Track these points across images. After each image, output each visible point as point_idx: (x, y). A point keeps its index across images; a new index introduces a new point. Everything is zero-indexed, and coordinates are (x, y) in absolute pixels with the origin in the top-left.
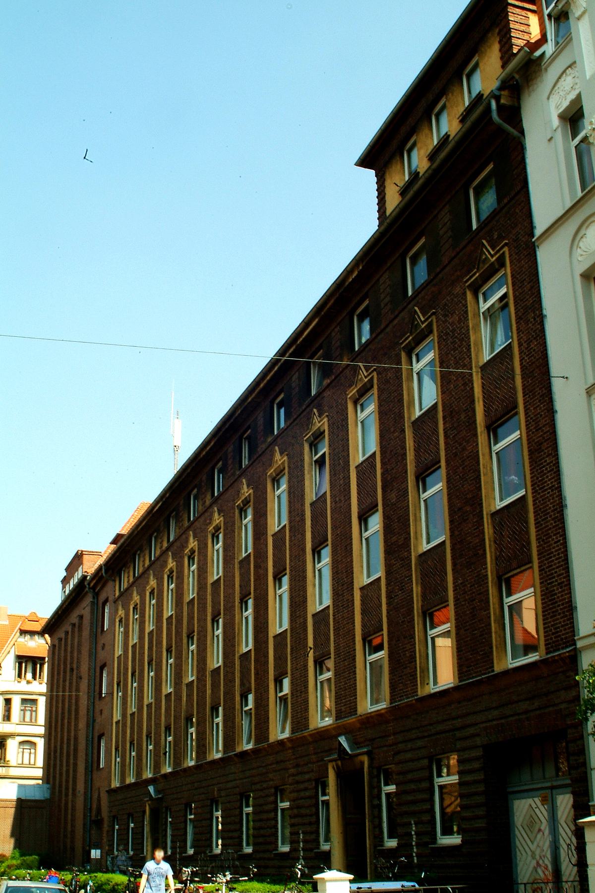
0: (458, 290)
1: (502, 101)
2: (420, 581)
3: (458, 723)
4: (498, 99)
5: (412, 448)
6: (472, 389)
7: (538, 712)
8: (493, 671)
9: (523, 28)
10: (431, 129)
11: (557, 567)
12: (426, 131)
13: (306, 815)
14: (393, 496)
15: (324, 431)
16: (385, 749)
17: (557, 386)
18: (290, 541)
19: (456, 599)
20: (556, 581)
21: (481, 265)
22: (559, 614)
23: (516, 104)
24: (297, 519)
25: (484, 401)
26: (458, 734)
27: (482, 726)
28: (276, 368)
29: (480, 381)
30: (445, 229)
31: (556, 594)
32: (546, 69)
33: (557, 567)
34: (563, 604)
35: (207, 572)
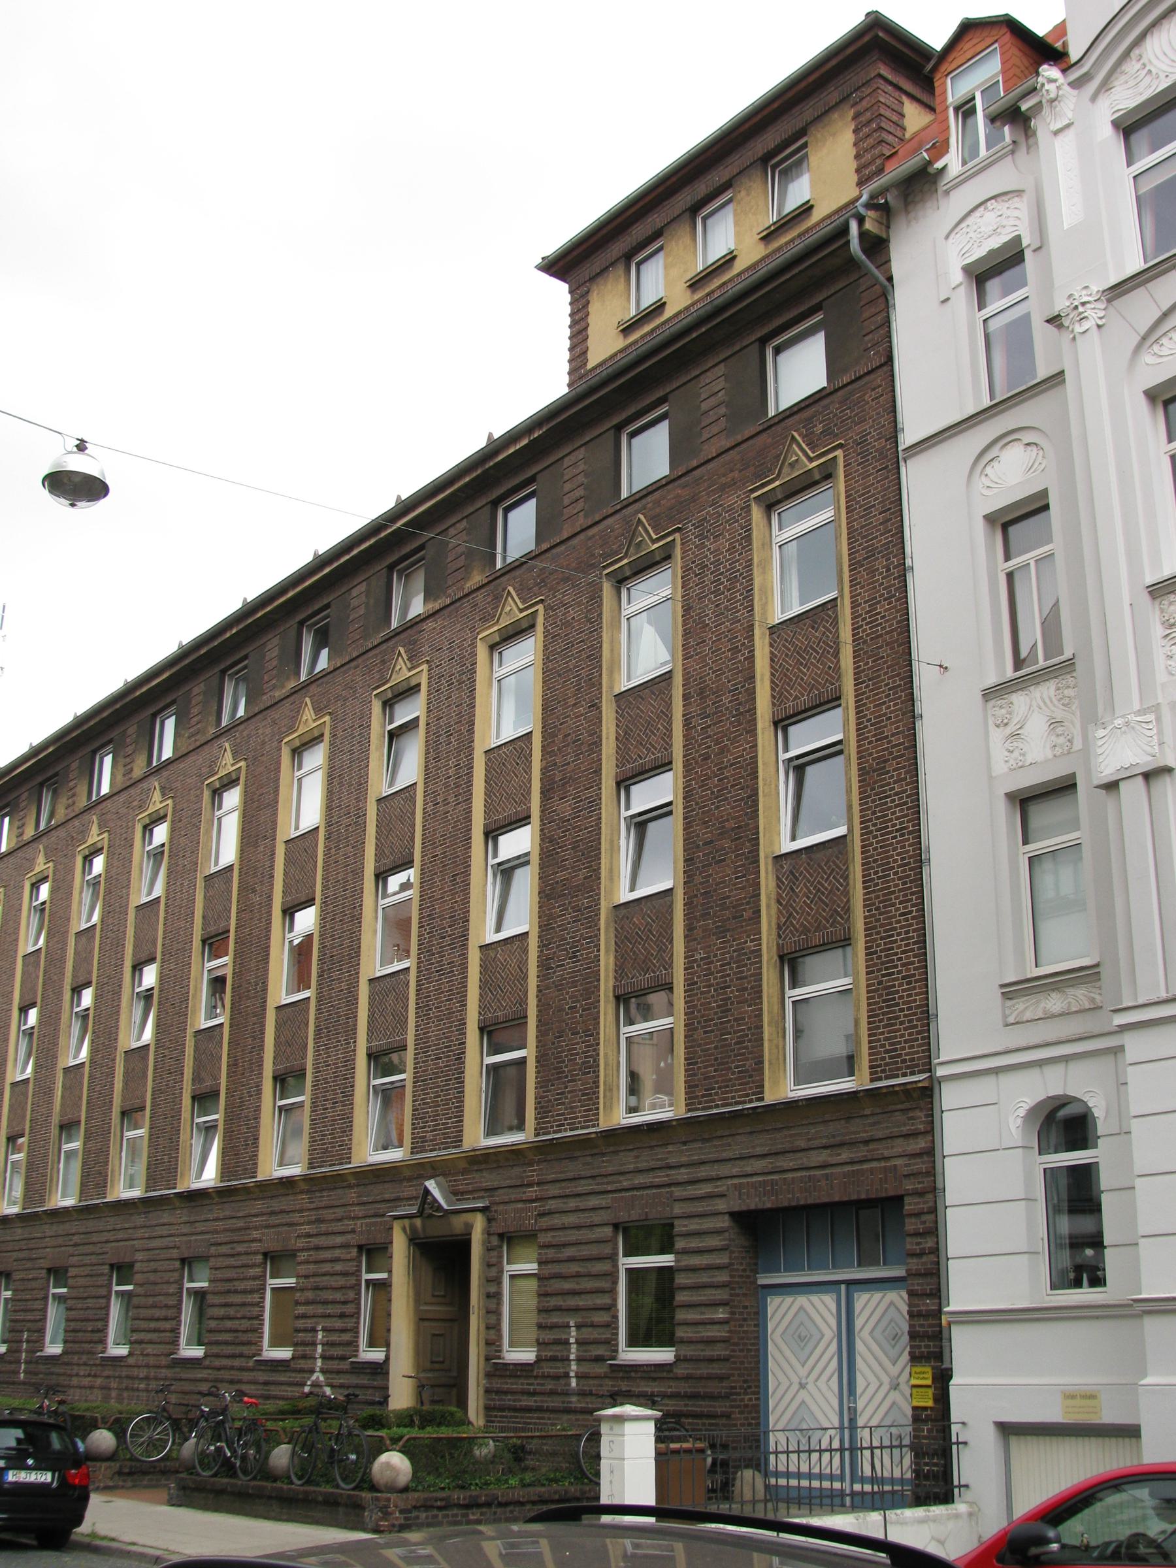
0: (733, 499)
1: (868, 225)
2: (613, 947)
3: (683, 1174)
4: (861, 220)
5: (613, 737)
6: (751, 658)
7: (847, 1168)
8: (762, 1099)
9: (895, 118)
10: (694, 240)
11: (903, 952)
12: (687, 240)
13: (334, 1302)
14: (564, 808)
15: (419, 685)
16: (520, 1205)
17: (925, 679)
18: (327, 853)
19: (690, 984)
20: (899, 972)
21: (786, 470)
22: (902, 1023)
23: (884, 236)
24: (346, 821)
25: (772, 682)
26: (678, 1192)
27: (730, 1182)
28: (327, 570)
29: (767, 649)
30: (712, 401)
31: (897, 992)
32: (947, 192)
33: (903, 952)
34: (909, 1009)
35: (128, 886)
